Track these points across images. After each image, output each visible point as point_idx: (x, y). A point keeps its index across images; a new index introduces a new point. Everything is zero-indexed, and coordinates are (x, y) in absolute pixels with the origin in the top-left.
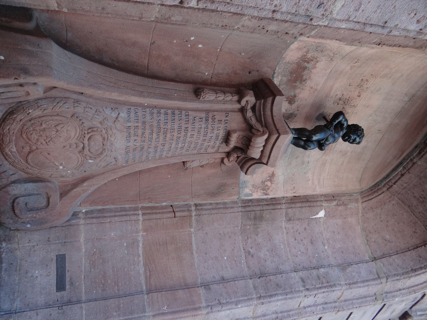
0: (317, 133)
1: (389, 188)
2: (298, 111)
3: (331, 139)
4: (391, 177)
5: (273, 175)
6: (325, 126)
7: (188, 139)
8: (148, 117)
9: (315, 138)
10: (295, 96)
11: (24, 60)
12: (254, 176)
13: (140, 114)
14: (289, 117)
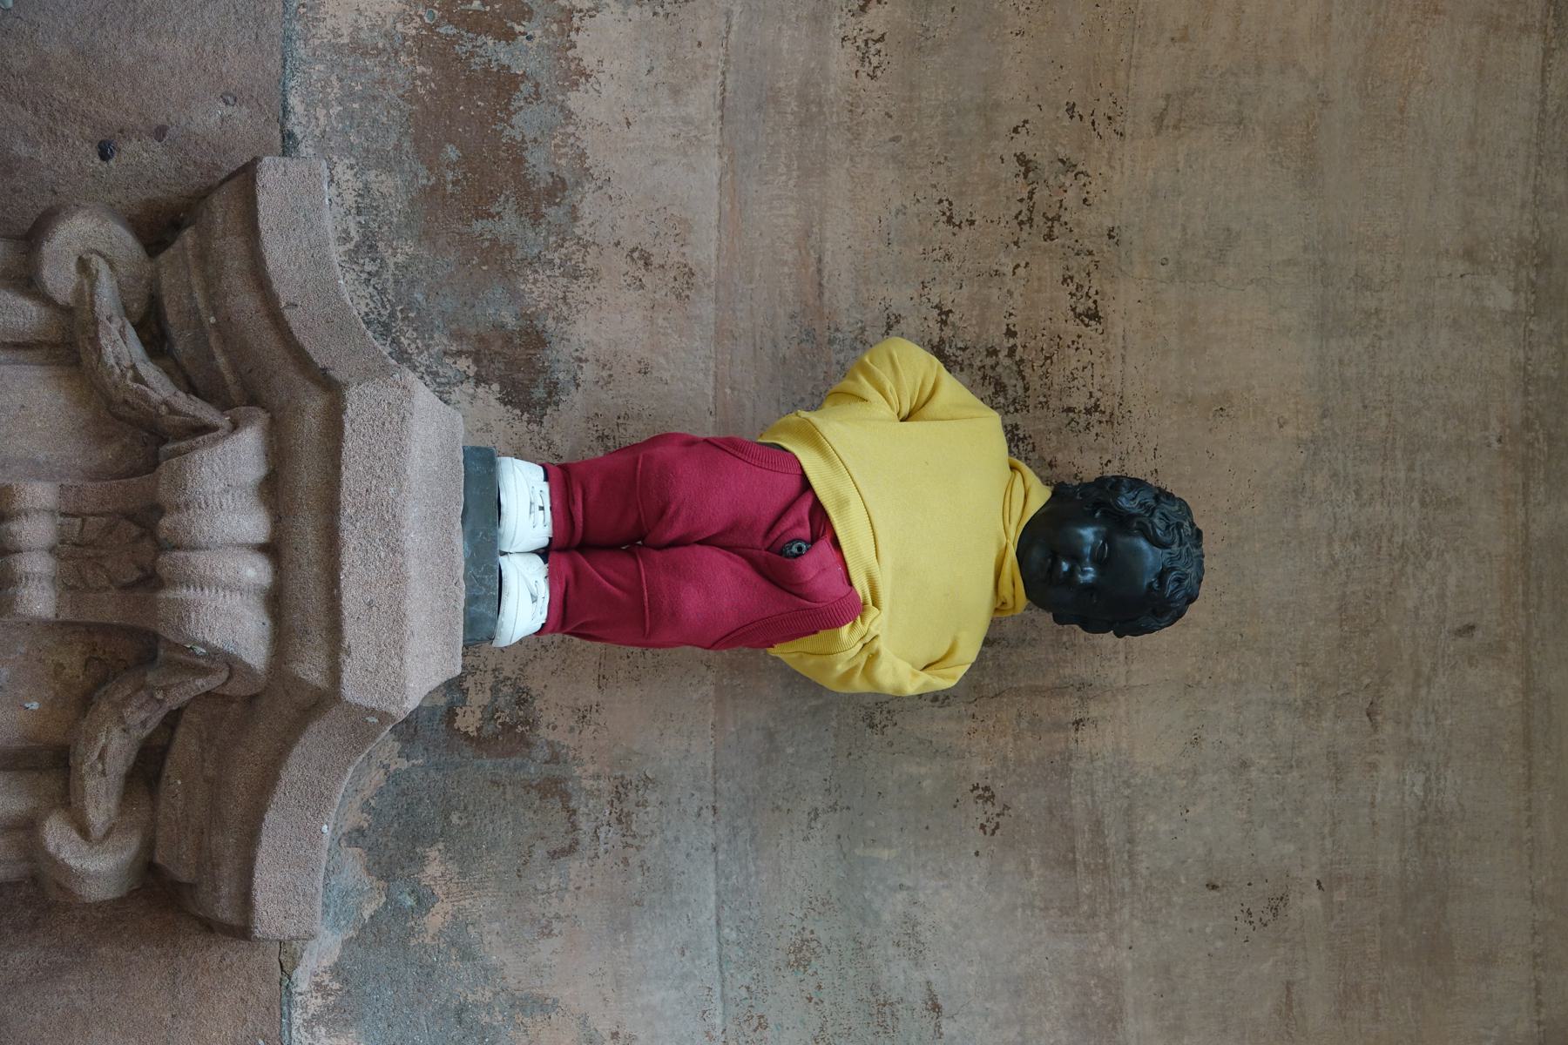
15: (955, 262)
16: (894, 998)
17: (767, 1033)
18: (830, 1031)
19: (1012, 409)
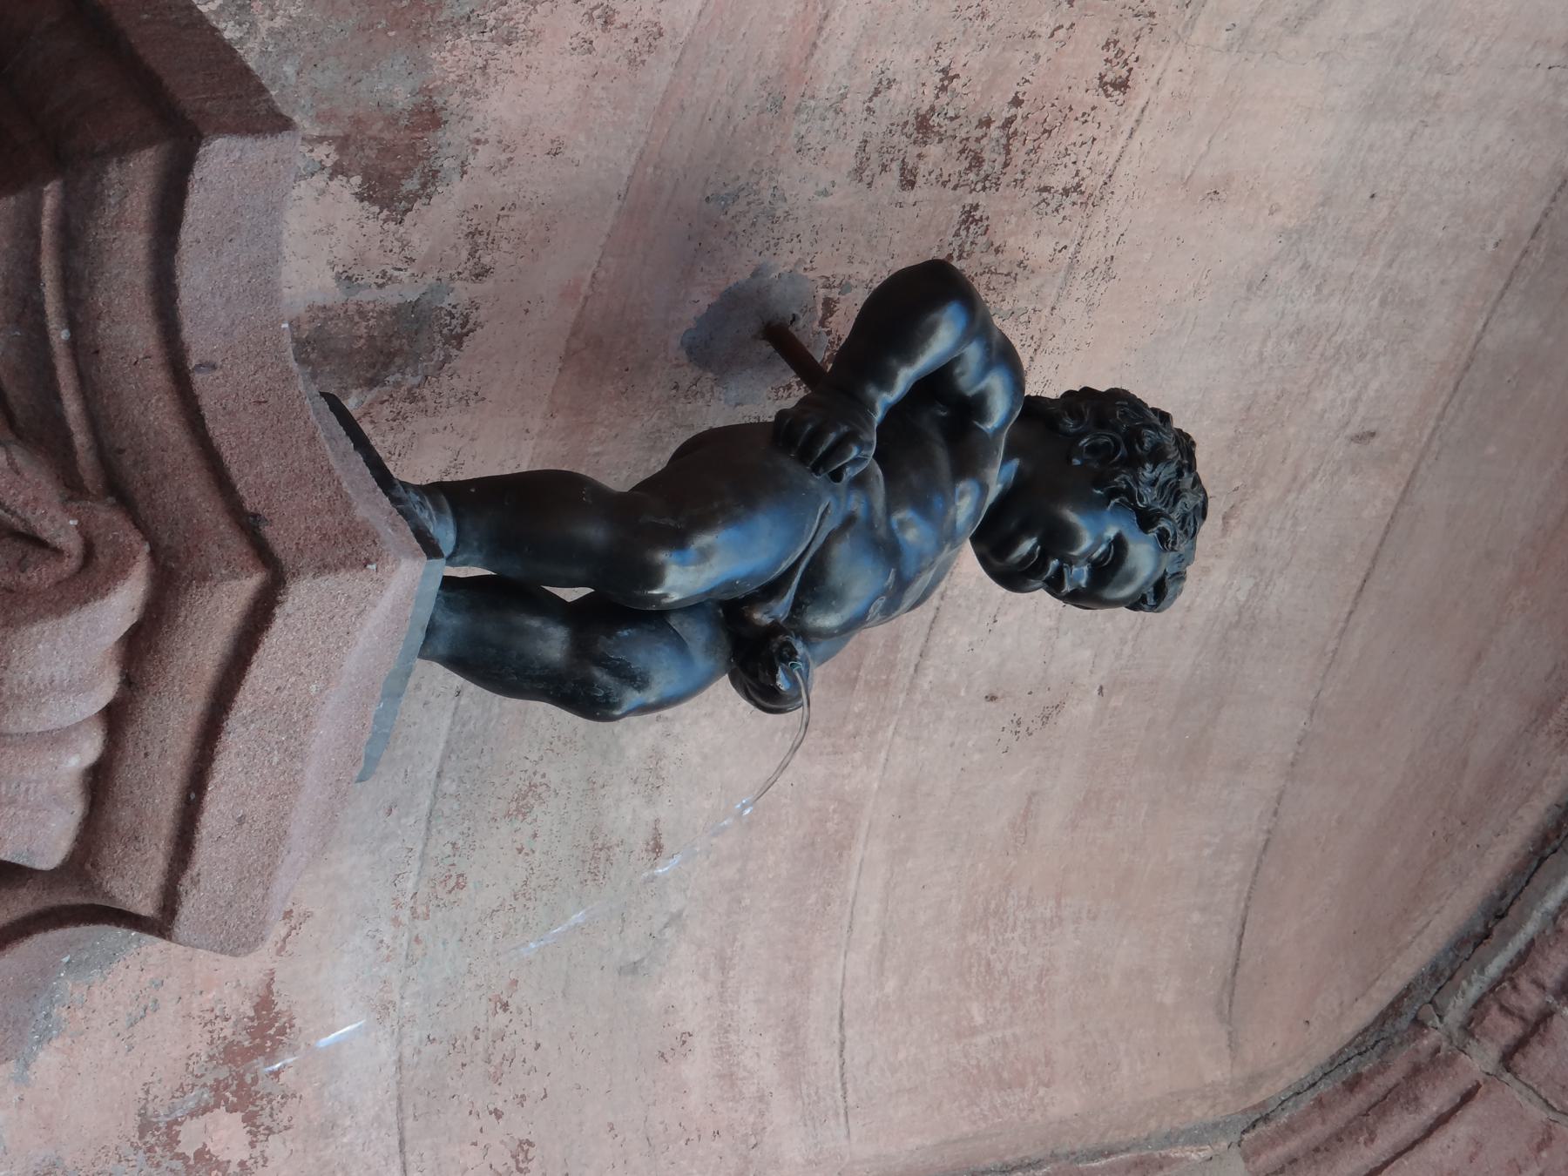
0: (704, 523)
1: (1521, 1044)
2: (481, 274)
3: (858, 579)
4: (1530, 928)
5: (266, 1027)
6: (786, 434)
9: (681, 579)
10: (429, 117)
12: (47, 1060)
14: (384, 348)
15: (988, 22)
16: (614, 840)
17: (463, 894)
18: (533, 885)
19: (979, 186)
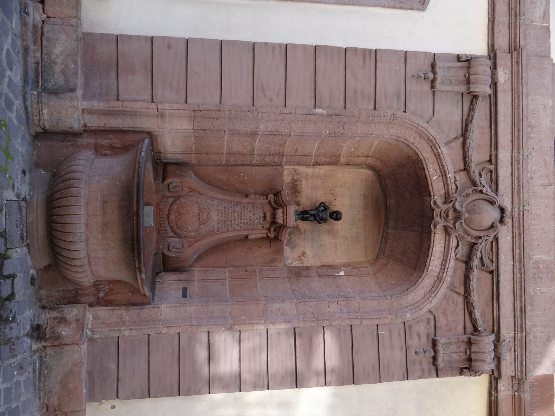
7: (246, 217)
8: (226, 205)
11: (184, 174)
13: (223, 203)
